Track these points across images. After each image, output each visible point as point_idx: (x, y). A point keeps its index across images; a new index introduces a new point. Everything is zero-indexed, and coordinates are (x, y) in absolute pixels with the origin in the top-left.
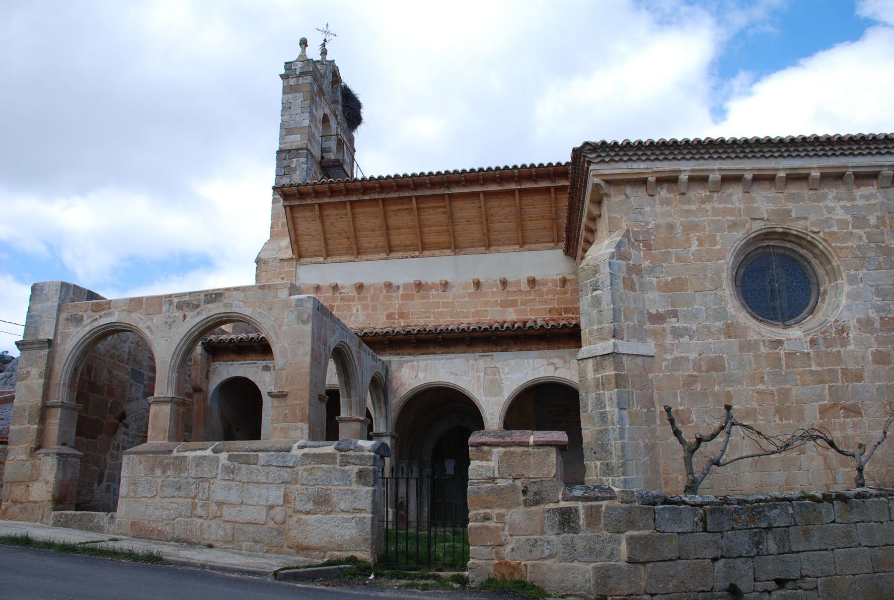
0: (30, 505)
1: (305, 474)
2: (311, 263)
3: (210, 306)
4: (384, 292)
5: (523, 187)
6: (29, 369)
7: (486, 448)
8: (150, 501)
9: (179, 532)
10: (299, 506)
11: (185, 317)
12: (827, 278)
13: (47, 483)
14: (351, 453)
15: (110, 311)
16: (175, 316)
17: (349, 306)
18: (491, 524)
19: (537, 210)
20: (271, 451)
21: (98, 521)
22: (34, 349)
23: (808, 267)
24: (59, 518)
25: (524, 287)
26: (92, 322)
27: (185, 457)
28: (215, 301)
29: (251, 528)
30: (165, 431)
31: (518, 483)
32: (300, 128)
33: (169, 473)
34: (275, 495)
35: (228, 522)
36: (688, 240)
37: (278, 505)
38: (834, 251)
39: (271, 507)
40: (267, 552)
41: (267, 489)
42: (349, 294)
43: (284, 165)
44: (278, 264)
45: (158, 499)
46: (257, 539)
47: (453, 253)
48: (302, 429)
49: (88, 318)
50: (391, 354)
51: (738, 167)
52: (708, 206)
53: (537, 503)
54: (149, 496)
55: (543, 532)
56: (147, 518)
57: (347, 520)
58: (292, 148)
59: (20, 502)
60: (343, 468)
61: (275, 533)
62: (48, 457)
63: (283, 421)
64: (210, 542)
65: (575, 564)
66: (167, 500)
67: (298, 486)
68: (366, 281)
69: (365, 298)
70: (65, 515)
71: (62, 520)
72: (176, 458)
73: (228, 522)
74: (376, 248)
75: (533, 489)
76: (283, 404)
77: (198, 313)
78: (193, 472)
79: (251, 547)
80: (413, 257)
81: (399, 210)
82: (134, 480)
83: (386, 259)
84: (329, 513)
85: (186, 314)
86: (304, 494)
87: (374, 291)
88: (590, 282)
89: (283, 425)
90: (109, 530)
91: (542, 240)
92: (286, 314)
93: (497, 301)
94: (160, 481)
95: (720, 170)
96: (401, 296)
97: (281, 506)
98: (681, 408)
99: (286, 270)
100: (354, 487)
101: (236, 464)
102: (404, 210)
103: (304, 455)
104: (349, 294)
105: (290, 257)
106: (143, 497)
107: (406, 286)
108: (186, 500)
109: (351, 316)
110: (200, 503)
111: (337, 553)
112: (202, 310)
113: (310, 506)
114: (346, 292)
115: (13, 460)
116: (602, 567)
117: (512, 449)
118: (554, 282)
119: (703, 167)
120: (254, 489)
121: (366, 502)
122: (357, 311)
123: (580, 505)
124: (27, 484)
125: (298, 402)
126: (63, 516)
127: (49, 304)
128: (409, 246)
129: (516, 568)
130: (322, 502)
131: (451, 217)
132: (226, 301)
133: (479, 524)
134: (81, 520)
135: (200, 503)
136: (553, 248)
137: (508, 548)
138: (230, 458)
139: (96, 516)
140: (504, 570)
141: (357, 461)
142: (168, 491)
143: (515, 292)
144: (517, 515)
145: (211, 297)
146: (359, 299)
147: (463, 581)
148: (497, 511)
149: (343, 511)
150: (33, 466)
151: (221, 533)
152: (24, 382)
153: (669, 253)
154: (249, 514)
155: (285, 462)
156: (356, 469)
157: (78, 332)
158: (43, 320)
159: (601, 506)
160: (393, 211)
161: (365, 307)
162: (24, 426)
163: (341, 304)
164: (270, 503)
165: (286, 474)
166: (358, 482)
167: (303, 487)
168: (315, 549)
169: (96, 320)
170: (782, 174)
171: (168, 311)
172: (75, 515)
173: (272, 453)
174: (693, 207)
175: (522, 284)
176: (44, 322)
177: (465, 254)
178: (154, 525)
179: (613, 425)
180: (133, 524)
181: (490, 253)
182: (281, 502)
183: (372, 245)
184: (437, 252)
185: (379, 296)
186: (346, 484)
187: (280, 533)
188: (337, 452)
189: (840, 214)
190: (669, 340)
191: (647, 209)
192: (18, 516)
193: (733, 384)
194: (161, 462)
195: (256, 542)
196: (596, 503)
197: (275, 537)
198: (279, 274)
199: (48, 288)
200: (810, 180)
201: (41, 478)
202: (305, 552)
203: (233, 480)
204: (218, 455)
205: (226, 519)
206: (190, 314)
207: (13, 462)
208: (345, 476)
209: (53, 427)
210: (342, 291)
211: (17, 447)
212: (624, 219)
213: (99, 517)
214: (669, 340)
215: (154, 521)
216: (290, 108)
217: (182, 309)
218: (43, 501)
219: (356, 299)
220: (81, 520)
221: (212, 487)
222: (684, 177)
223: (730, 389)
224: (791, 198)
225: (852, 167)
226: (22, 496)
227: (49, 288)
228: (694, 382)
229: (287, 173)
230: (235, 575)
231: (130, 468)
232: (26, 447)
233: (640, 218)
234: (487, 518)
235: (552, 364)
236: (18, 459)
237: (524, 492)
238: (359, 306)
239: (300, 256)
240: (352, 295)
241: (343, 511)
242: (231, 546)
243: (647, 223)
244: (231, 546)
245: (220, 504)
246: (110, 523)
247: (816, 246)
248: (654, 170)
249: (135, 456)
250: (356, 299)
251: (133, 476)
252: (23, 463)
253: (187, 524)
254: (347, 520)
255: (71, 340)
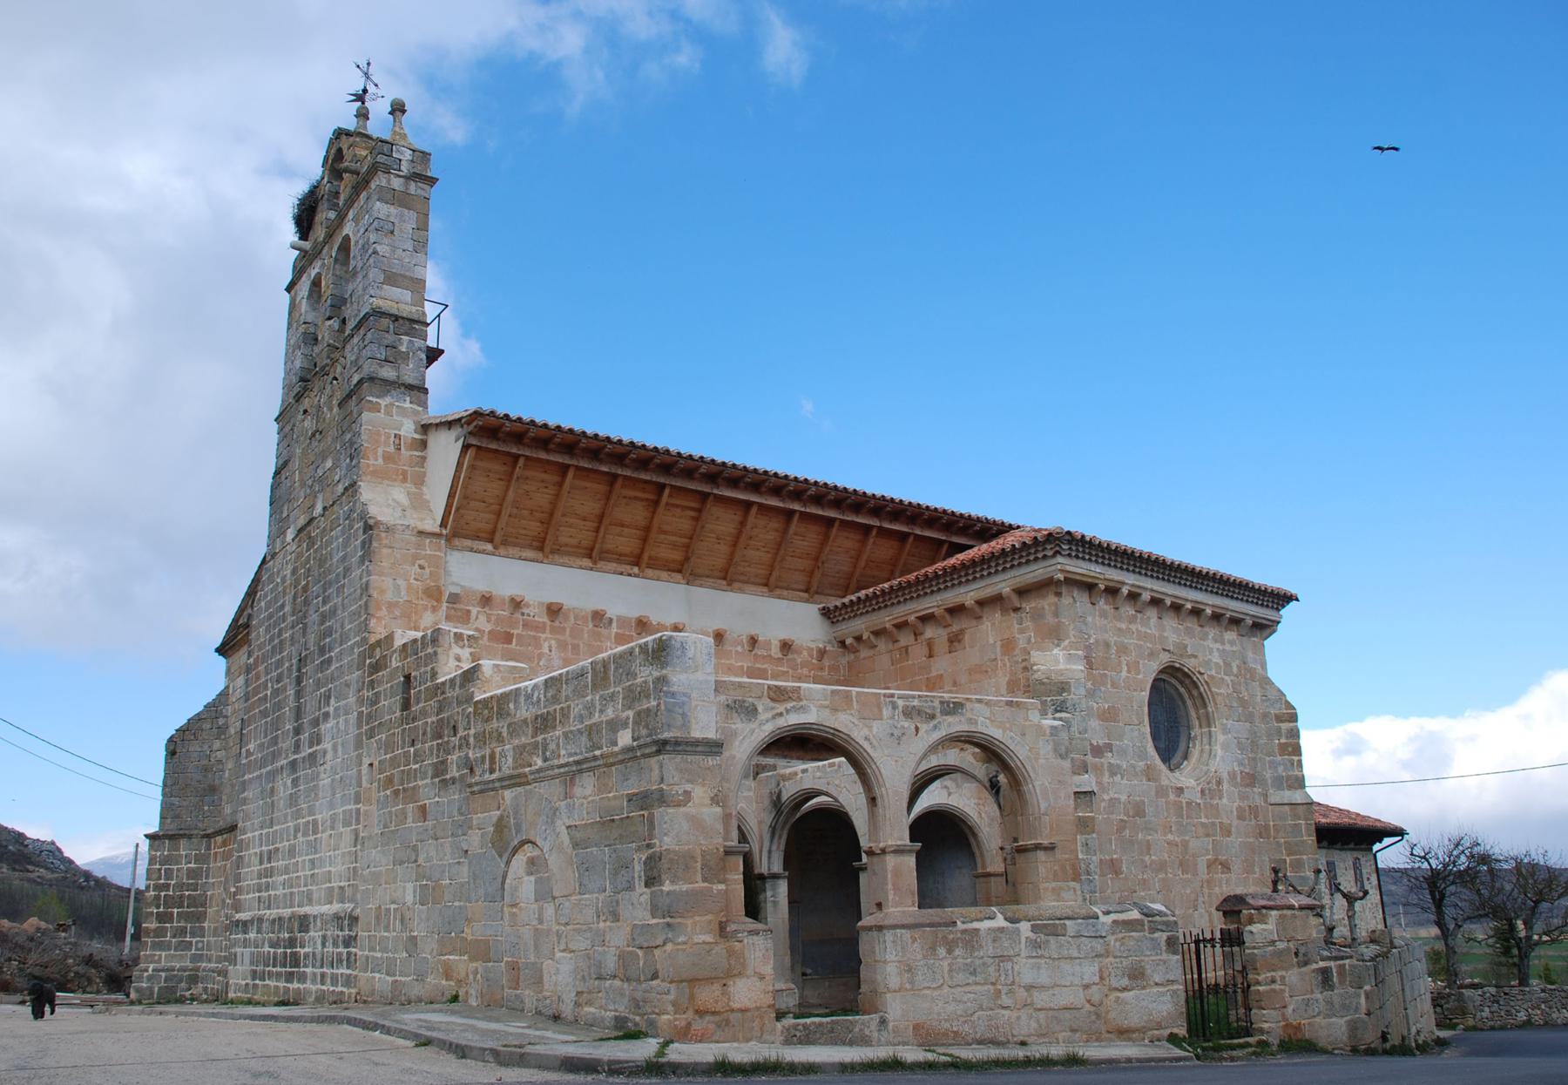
0: (732, 1017)
1: (1118, 944)
2: (471, 550)
3: (950, 719)
4: (591, 626)
5: (808, 510)
6: (688, 787)
7: (1264, 911)
8: (936, 993)
9: (982, 1031)
10: (1115, 984)
11: (917, 729)
12: (1197, 723)
13: (762, 978)
14: (1158, 918)
15: (801, 703)
16: (903, 727)
17: (536, 639)
18: (1277, 987)
19: (806, 543)
20: (1077, 918)
21: (861, 1030)
22: (696, 753)
23: (1182, 707)
24: (793, 1032)
25: (775, 651)
26: (774, 717)
27: (977, 930)
28: (954, 713)
29: (1067, 1015)
30: (913, 894)
31: (1291, 944)
32: (411, 279)
33: (957, 952)
34: (1090, 971)
35: (1040, 1010)
36: (1120, 663)
37: (1094, 984)
38: (1213, 696)
39: (1086, 987)
40: (1087, 1041)
41: (1080, 965)
42: (536, 618)
43: (386, 342)
44: (413, 539)
45: (946, 990)
46: (1075, 1027)
47: (685, 582)
48: (1075, 891)
49: (766, 710)
50: (776, 755)
51: (1163, 590)
52: (1133, 627)
53: (1306, 963)
54: (935, 986)
55: (1312, 992)
56: (936, 1017)
57: (1163, 994)
58: (401, 314)
59: (714, 1013)
60: (1152, 936)
61: (1093, 1017)
62: (755, 938)
63: (1054, 881)
64: (1022, 1038)
65: (1334, 1019)
66: (959, 989)
67: (1111, 959)
68: (568, 601)
69: (562, 630)
70: (804, 1025)
71: (798, 1035)
72: (964, 931)
73: (1040, 1010)
74: (578, 547)
75: (1302, 950)
76: (1051, 859)
77: (935, 727)
78: (989, 949)
79: (1070, 1037)
80: (630, 575)
81: (636, 498)
82: (909, 965)
83: (591, 569)
84: (1144, 988)
85: (919, 725)
86: (1118, 968)
87: (575, 620)
88: (1052, 700)
89: (1054, 884)
90: (879, 1040)
91: (795, 586)
92: (1041, 743)
93: (742, 667)
94: (945, 964)
95: (1152, 590)
96: (615, 637)
97: (1097, 984)
98: (1115, 856)
99: (428, 552)
100: (1165, 956)
101: (1042, 936)
102: (642, 500)
103: (1115, 922)
104: (536, 618)
105: (437, 530)
106: (924, 988)
107: (623, 621)
108: (986, 987)
109: (540, 656)
110: (1004, 990)
111: (1155, 1032)
112: (939, 723)
113: (1125, 982)
114: (532, 614)
115: (685, 943)
116: (1351, 1020)
117: (1285, 912)
118: (810, 650)
119: (1141, 584)
120: (1066, 966)
121: (1177, 973)
122: (550, 651)
123: (1332, 964)
124: (724, 981)
125: (1067, 856)
126: (800, 1027)
127: (700, 676)
128: (626, 555)
129: (1298, 1028)
130: (1137, 975)
131: (742, 524)
132: (969, 715)
133: (1268, 987)
134: (832, 1031)
135: (1004, 990)
136: (807, 601)
137: (1290, 1008)
138: (1034, 929)
139: (857, 1022)
140: (1290, 1031)
141: (1164, 928)
142: (960, 977)
143: (764, 657)
144: (1293, 976)
145: (948, 706)
146: (553, 630)
147: (1263, 1044)
148: (1280, 973)
149: (1156, 984)
150: (731, 953)
151: (1034, 1025)
152: (682, 809)
153: (1105, 675)
154: (1066, 997)
155: (1097, 931)
156: (1164, 936)
157: (753, 731)
158: (694, 704)
159: (1345, 965)
160: (625, 497)
161: (562, 646)
162: (697, 885)
163: (524, 633)
164: (1085, 982)
165: (1098, 946)
166: (1168, 951)
167: (1118, 960)
168: (1133, 1031)
169: (781, 714)
170: (1189, 606)
171: (892, 718)
172: (821, 1024)
173: (1080, 921)
174: (1123, 626)
175: (773, 647)
176: (696, 706)
177: (701, 586)
178: (947, 1025)
179: (1089, 875)
180: (916, 1027)
181: (732, 591)
182: (1097, 979)
183: (574, 541)
184: (664, 574)
185: (582, 630)
186: (1157, 954)
187: (1098, 1016)
188: (1143, 917)
189: (1216, 658)
190: (1106, 779)
191: (1089, 619)
192: (712, 1034)
193: (1152, 832)
194: (944, 937)
195: (1073, 1031)
196: (1341, 962)
197: (1094, 1022)
198: (415, 557)
199: (693, 649)
200: (1203, 617)
201: (750, 972)
202: (1125, 1036)
203: (1042, 957)
204: (1017, 925)
205: (1039, 1006)
206: (924, 727)
207: (684, 947)
208: (1155, 945)
209: (733, 886)
210: (526, 611)
211: (689, 922)
212: (1072, 627)
213: (863, 1024)
214: (1106, 779)
215: (946, 1020)
216: (392, 232)
217: (911, 718)
218: (758, 1008)
219: (548, 628)
220: (832, 1031)
221: (1016, 968)
222: (1125, 590)
223: (1150, 837)
224: (1189, 632)
225: (1232, 611)
226: (717, 1002)
227: (696, 647)
228: (1124, 828)
229: (391, 359)
230: (1167, 1063)
231: (899, 948)
232: (710, 922)
233: (1084, 628)
234: (1273, 981)
235: (946, 787)
236: (696, 941)
237: (1296, 954)
238: (553, 642)
239: (455, 534)
240: (541, 620)
241: (1156, 984)
242: (1047, 1040)
243: (1090, 636)
244: (1047, 1040)
245: (1029, 988)
246: (880, 1030)
247: (1197, 687)
248: (1107, 576)
249: (903, 931)
250: (548, 628)
251: (905, 959)
252: (707, 947)
253: (990, 1018)
254: (1163, 994)
255: (741, 742)
